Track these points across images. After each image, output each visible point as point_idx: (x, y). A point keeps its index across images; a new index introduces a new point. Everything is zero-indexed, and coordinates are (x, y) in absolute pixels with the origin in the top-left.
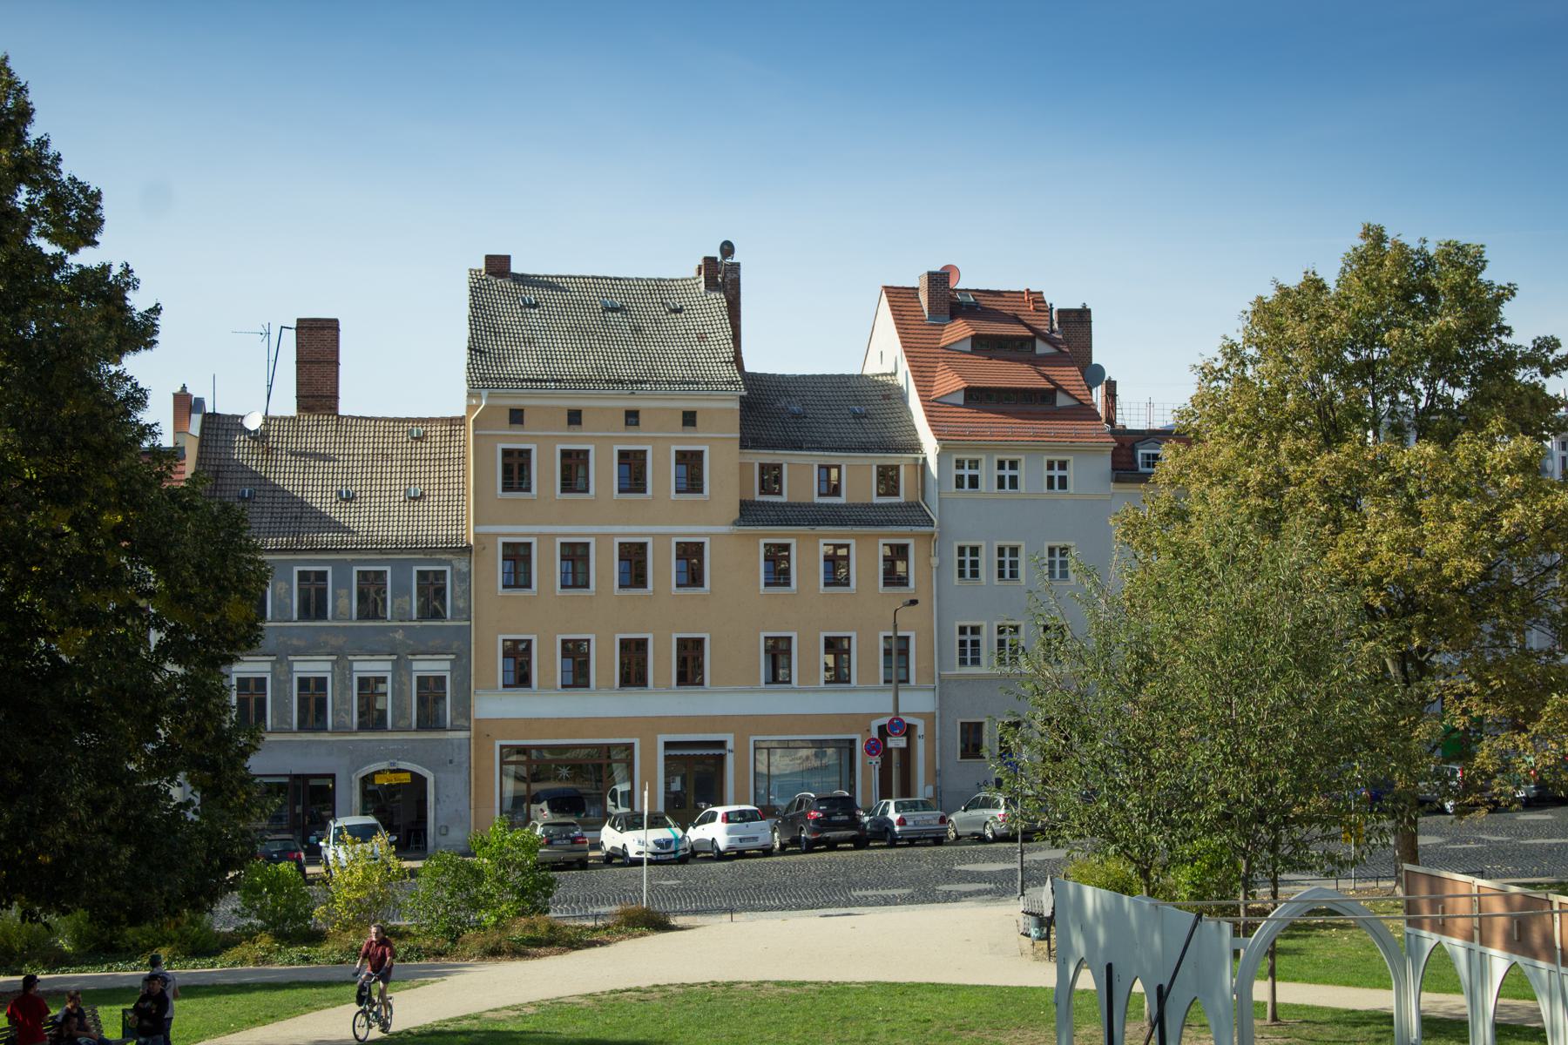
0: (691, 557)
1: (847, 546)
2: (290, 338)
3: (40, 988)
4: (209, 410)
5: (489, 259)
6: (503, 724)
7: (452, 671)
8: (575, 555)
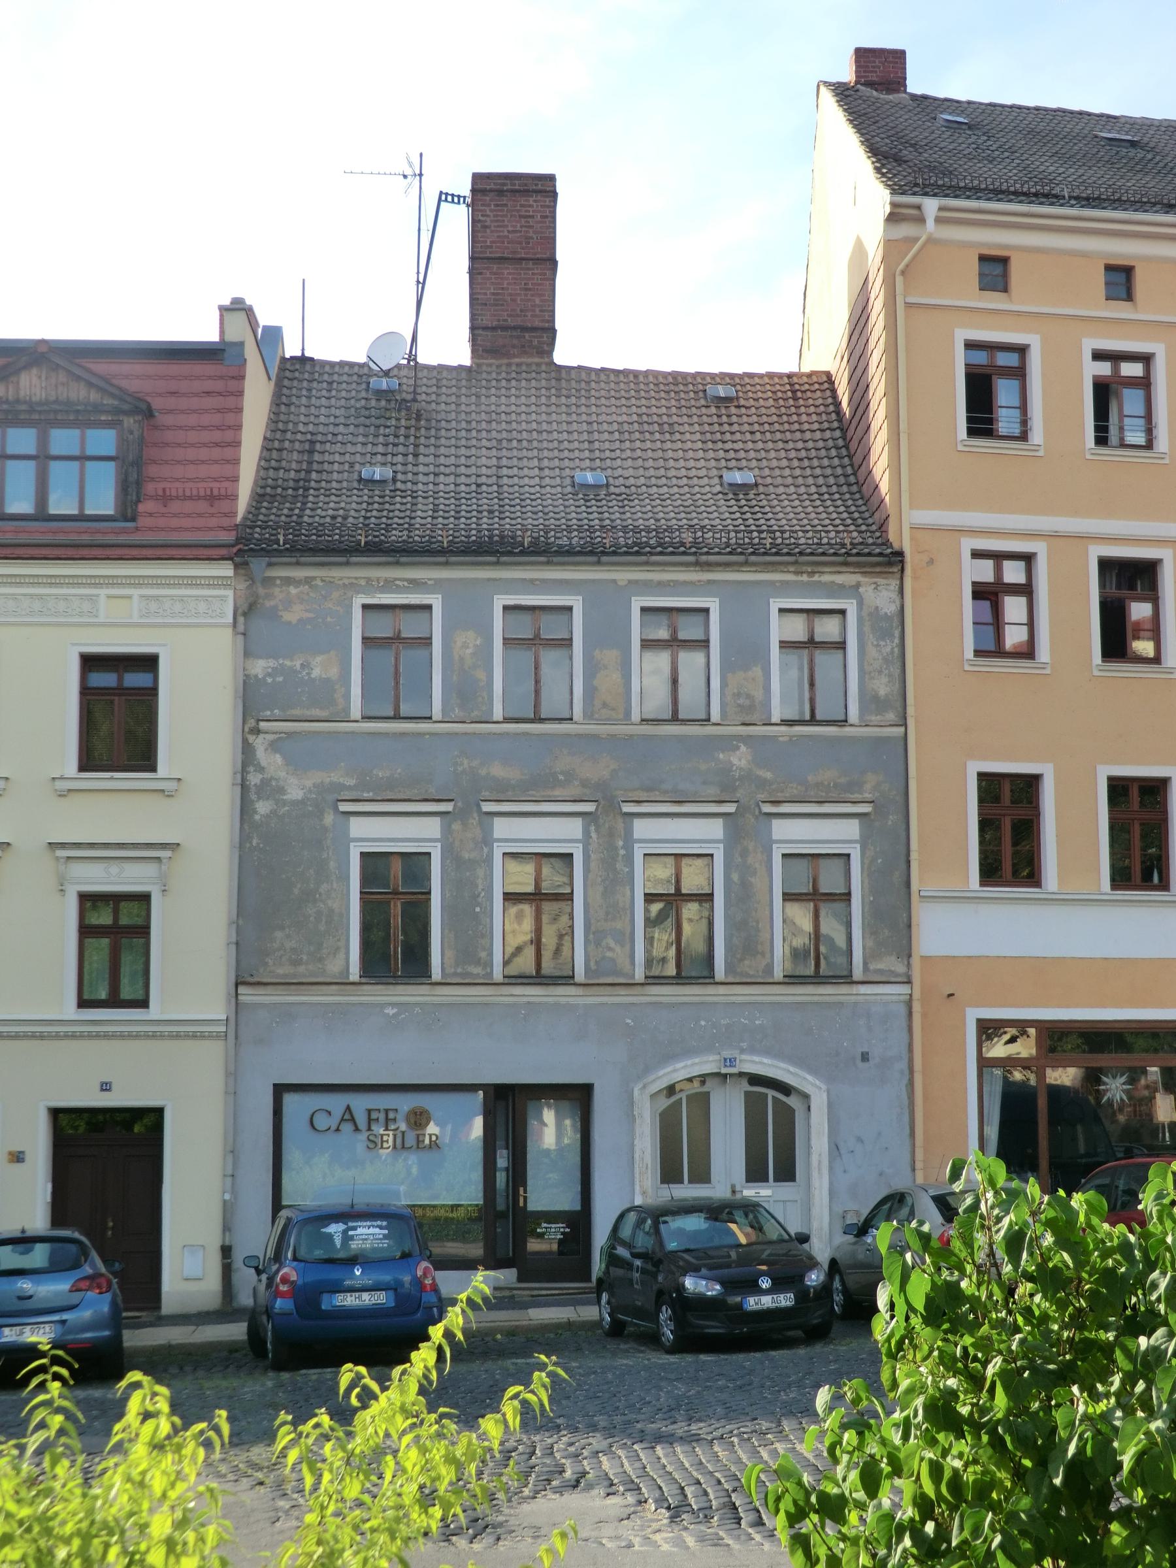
2: (456, 225)
3: (84, 1530)
4: (292, 350)
5: (863, 56)
6: (989, 972)
7: (864, 842)
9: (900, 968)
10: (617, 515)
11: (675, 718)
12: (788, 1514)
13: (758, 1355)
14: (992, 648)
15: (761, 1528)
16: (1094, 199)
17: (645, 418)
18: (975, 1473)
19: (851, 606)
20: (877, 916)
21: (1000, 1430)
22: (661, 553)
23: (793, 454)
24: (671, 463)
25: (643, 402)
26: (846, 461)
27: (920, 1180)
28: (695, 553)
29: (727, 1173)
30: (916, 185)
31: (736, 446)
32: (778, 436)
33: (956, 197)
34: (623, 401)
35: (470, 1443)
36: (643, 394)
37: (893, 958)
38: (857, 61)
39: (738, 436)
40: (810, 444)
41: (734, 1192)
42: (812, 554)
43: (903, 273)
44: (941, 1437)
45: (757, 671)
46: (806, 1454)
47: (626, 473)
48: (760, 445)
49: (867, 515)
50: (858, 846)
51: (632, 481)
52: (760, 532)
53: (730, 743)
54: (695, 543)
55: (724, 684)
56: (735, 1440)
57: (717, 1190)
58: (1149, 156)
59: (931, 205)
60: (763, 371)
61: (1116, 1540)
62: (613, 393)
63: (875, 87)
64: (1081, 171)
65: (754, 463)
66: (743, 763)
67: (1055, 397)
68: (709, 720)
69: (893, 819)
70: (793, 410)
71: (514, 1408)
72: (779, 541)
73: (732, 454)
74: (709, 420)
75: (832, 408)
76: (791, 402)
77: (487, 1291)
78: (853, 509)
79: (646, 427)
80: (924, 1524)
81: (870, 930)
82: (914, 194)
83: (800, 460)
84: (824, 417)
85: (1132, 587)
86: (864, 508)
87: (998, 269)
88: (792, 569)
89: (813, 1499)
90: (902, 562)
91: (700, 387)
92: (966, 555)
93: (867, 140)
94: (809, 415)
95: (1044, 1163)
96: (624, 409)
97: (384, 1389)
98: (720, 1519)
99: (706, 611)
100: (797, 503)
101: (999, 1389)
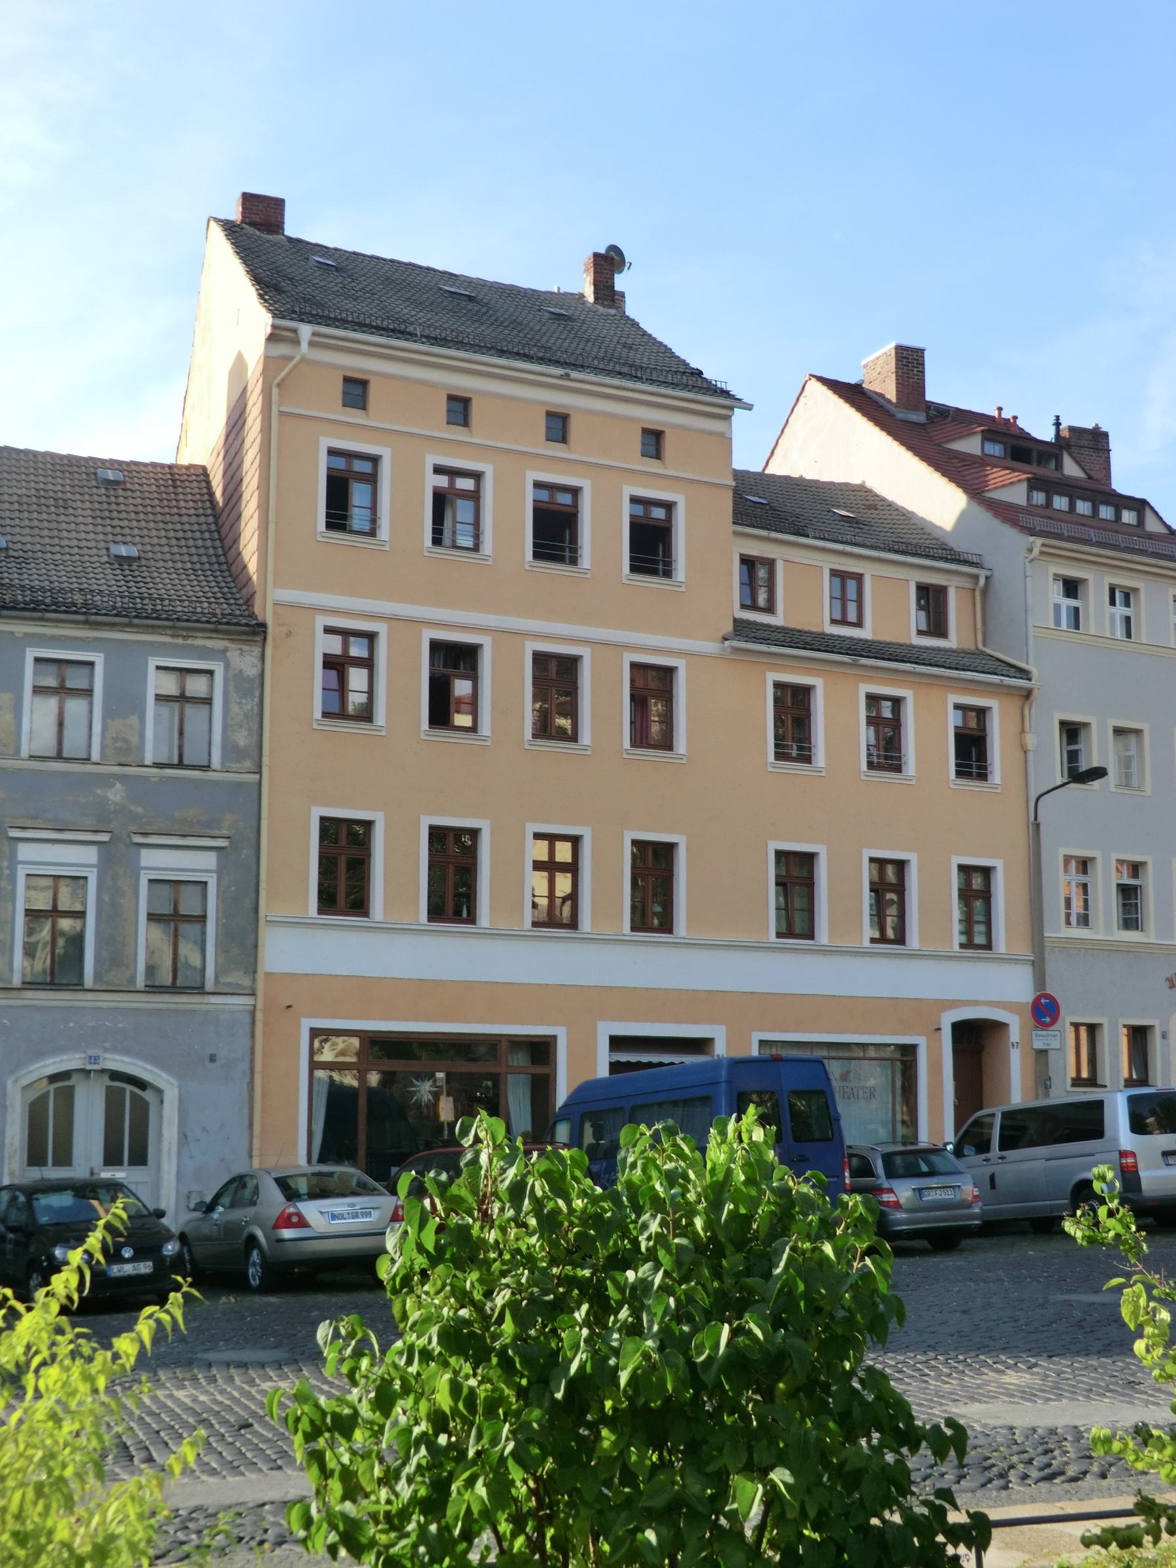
0: (652, 687)
1: (371, 637)
5: (249, 200)
7: (220, 872)
8: (556, 677)
9: (247, 982)
10: (16, 575)
11: (59, 757)
12: (305, 1434)
13: (122, 1316)
14: (337, 711)
15: (152, 1464)
16: (441, 339)
17: (42, 493)
18: (486, 1390)
19: (218, 668)
20: (227, 936)
21: (510, 1352)
22: (55, 611)
23: (172, 534)
24: (65, 534)
25: (41, 479)
26: (218, 543)
27: (256, 1164)
28: (85, 613)
29: (87, 1154)
30: (294, 312)
31: (122, 524)
32: (159, 517)
33: (327, 325)
34: (23, 477)
35: (105, 1361)
36: (41, 471)
37: (241, 973)
38: (243, 204)
39: (124, 515)
40: (187, 527)
41: (92, 1174)
42: (187, 621)
43: (279, 385)
44: (453, 1361)
45: (134, 720)
46: (184, 1399)
47: (24, 540)
48: (143, 524)
49: (235, 590)
50: (215, 875)
51: (29, 547)
52: (142, 599)
53: (106, 780)
54: (85, 605)
55: (105, 729)
56: (118, 1388)
57: (78, 1171)
58: (484, 310)
59: (306, 331)
60: (147, 461)
61: (606, 1444)
62: (14, 469)
63: (257, 225)
64: (429, 316)
65: (138, 539)
66: (118, 798)
67: (400, 500)
68: (89, 759)
69: (246, 853)
70: (173, 496)
71: (150, 1327)
72: (159, 607)
73: (118, 530)
74: (99, 499)
75: (206, 497)
76: (171, 489)
77: (124, 1215)
78: (223, 584)
79: (43, 501)
80: (437, 1436)
81: (221, 947)
82: (292, 319)
83: (178, 539)
84: (200, 504)
85: (456, 667)
86: (232, 585)
87: (358, 390)
88: (169, 632)
89: (328, 1420)
90: (265, 632)
91: (92, 470)
92: (319, 630)
93: (252, 270)
94: (186, 501)
95: (362, 1153)
96: (24, 484)
97: (29, 1309)
98: (115, 1457)
99: (91, 664)
100: (174, 576)
101: (508, 1317)
